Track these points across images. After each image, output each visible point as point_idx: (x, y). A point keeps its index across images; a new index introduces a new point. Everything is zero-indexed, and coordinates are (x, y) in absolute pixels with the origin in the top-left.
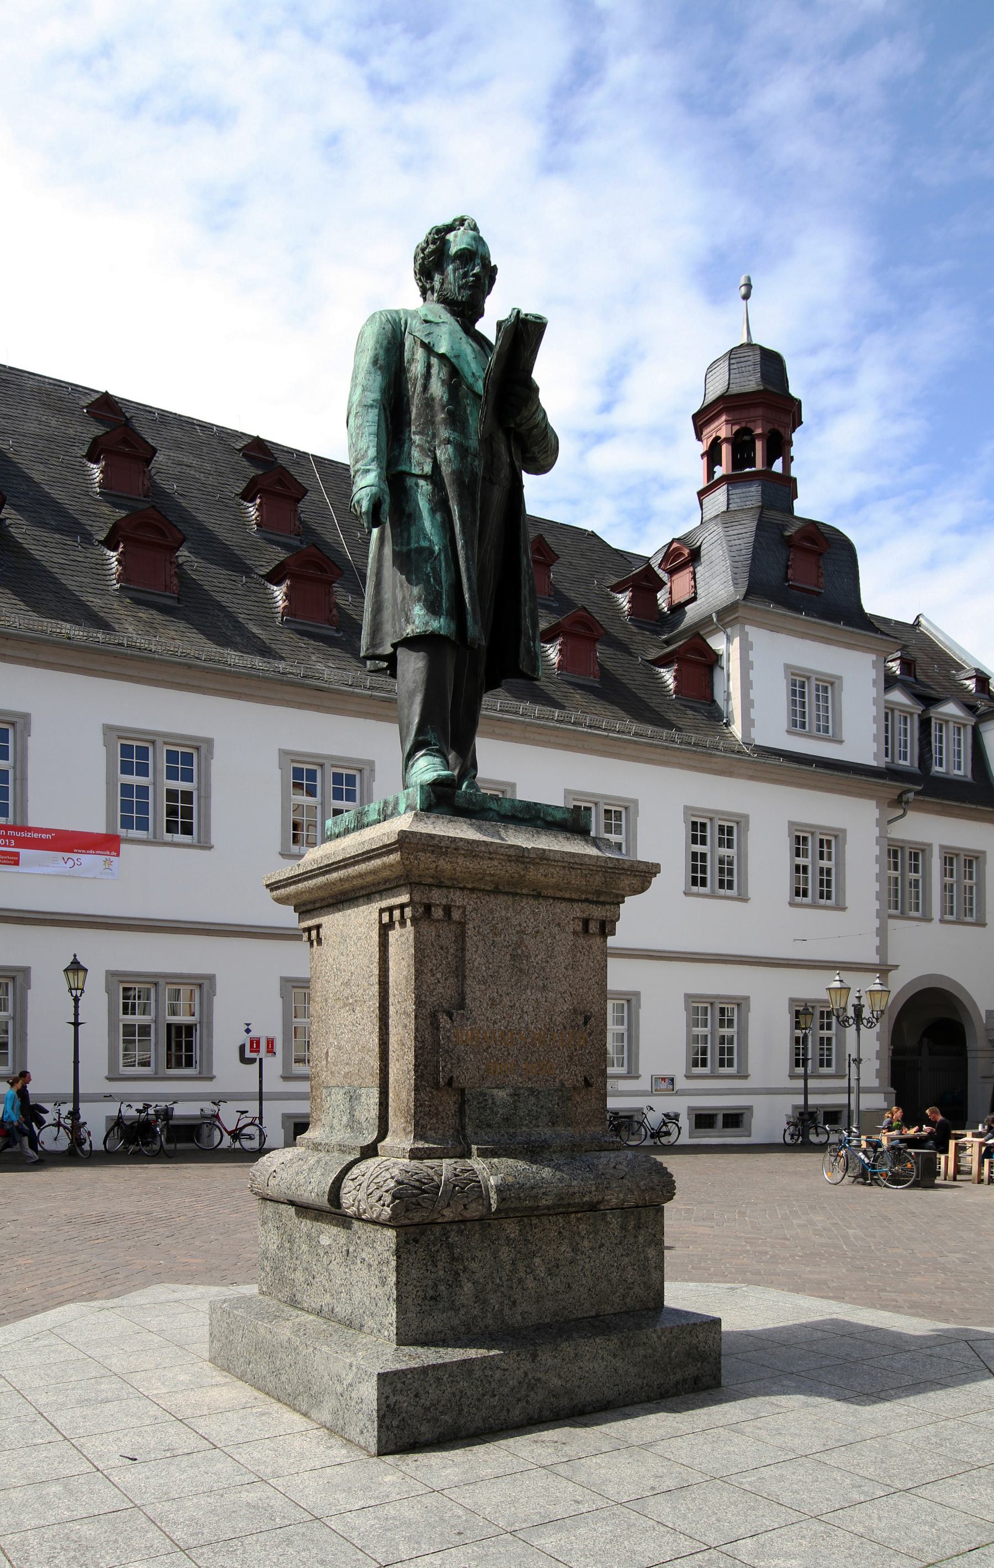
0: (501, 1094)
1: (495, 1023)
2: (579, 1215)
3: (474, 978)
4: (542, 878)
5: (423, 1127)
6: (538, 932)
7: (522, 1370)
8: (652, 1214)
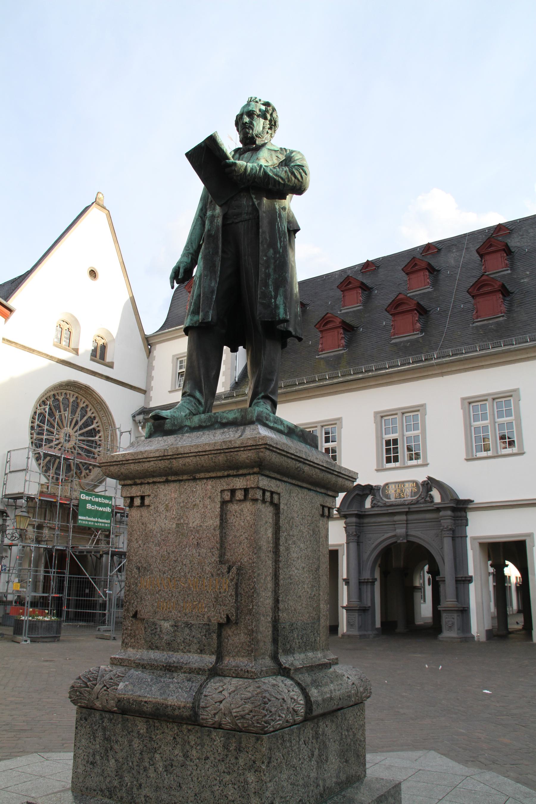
1: (164, 573)
3: (153, 542)
6: (195, 505)
8: (253, 740)
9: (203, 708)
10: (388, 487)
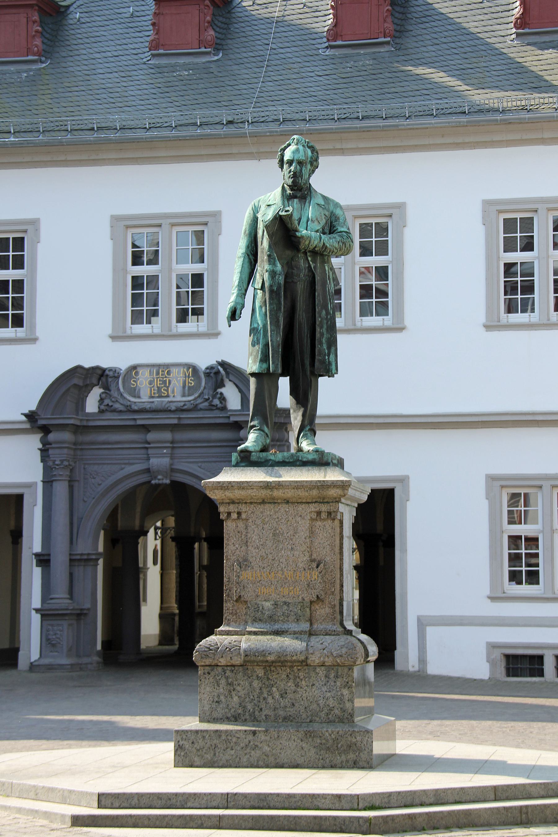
0: (268, 605)
1: (264, 568)
2: (299, 668)
4: (283, 495)
5: (228, 620)
7: (247, 739)
9: (312, 654)
10: (137, 374)
